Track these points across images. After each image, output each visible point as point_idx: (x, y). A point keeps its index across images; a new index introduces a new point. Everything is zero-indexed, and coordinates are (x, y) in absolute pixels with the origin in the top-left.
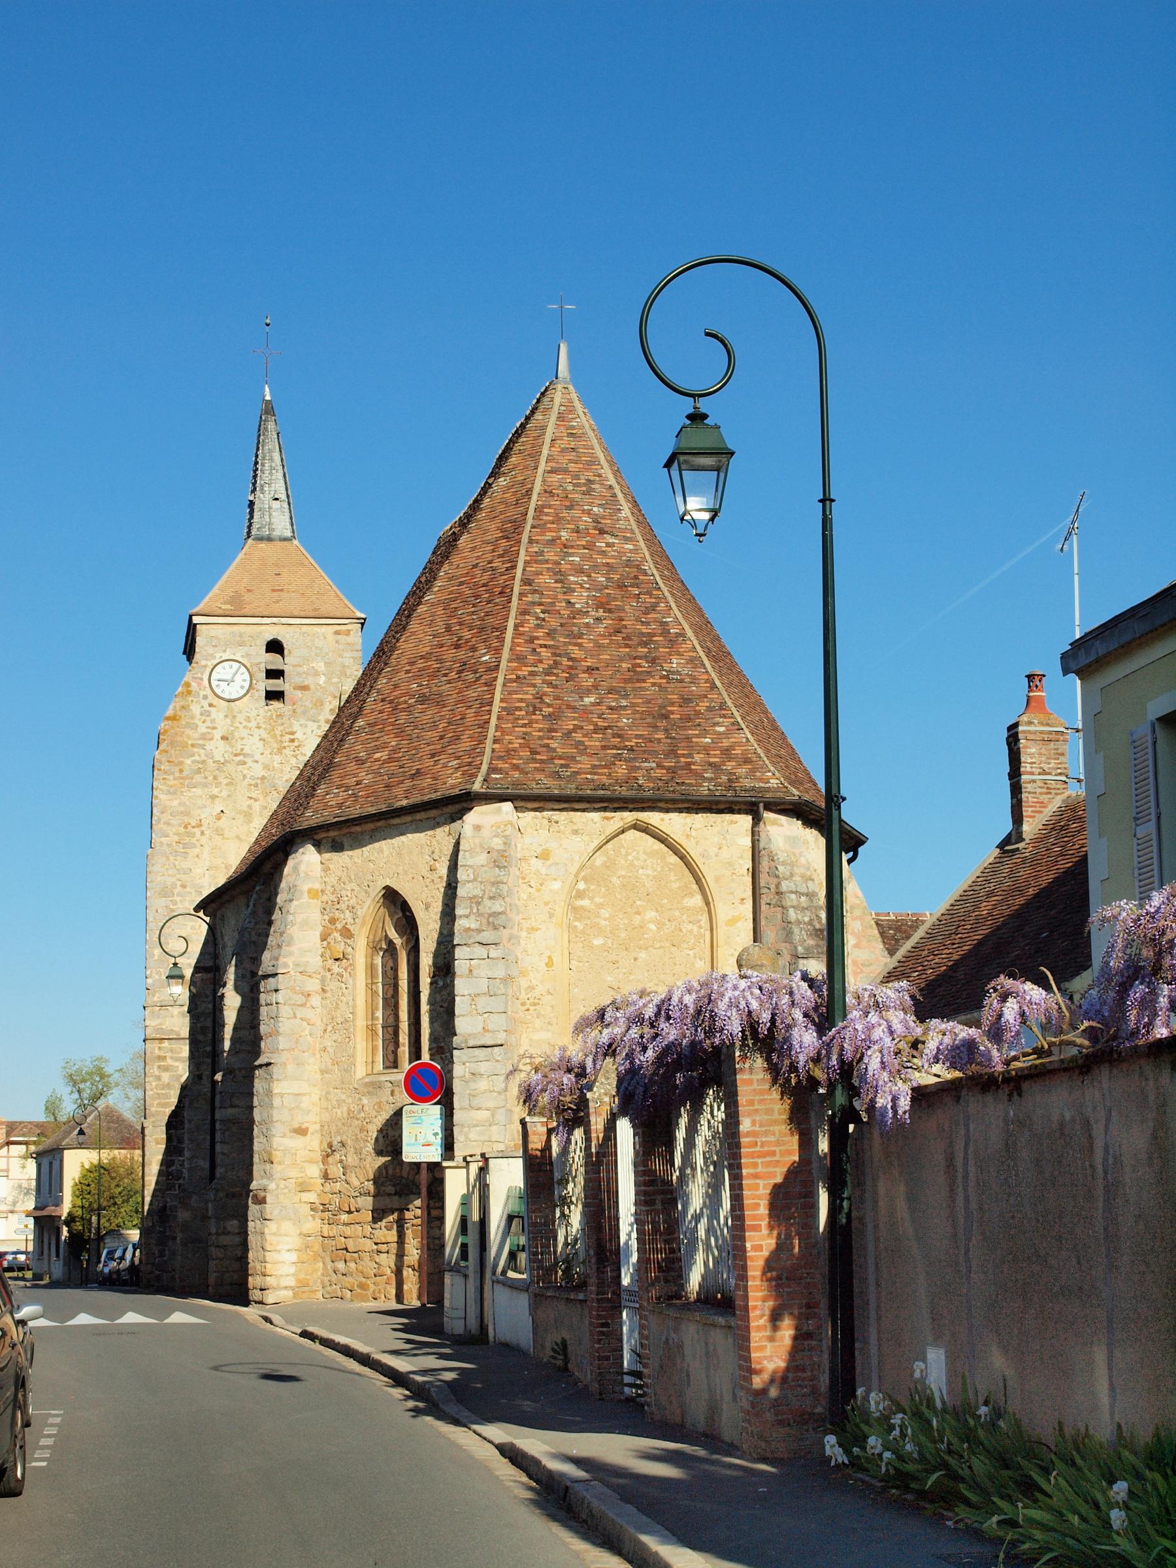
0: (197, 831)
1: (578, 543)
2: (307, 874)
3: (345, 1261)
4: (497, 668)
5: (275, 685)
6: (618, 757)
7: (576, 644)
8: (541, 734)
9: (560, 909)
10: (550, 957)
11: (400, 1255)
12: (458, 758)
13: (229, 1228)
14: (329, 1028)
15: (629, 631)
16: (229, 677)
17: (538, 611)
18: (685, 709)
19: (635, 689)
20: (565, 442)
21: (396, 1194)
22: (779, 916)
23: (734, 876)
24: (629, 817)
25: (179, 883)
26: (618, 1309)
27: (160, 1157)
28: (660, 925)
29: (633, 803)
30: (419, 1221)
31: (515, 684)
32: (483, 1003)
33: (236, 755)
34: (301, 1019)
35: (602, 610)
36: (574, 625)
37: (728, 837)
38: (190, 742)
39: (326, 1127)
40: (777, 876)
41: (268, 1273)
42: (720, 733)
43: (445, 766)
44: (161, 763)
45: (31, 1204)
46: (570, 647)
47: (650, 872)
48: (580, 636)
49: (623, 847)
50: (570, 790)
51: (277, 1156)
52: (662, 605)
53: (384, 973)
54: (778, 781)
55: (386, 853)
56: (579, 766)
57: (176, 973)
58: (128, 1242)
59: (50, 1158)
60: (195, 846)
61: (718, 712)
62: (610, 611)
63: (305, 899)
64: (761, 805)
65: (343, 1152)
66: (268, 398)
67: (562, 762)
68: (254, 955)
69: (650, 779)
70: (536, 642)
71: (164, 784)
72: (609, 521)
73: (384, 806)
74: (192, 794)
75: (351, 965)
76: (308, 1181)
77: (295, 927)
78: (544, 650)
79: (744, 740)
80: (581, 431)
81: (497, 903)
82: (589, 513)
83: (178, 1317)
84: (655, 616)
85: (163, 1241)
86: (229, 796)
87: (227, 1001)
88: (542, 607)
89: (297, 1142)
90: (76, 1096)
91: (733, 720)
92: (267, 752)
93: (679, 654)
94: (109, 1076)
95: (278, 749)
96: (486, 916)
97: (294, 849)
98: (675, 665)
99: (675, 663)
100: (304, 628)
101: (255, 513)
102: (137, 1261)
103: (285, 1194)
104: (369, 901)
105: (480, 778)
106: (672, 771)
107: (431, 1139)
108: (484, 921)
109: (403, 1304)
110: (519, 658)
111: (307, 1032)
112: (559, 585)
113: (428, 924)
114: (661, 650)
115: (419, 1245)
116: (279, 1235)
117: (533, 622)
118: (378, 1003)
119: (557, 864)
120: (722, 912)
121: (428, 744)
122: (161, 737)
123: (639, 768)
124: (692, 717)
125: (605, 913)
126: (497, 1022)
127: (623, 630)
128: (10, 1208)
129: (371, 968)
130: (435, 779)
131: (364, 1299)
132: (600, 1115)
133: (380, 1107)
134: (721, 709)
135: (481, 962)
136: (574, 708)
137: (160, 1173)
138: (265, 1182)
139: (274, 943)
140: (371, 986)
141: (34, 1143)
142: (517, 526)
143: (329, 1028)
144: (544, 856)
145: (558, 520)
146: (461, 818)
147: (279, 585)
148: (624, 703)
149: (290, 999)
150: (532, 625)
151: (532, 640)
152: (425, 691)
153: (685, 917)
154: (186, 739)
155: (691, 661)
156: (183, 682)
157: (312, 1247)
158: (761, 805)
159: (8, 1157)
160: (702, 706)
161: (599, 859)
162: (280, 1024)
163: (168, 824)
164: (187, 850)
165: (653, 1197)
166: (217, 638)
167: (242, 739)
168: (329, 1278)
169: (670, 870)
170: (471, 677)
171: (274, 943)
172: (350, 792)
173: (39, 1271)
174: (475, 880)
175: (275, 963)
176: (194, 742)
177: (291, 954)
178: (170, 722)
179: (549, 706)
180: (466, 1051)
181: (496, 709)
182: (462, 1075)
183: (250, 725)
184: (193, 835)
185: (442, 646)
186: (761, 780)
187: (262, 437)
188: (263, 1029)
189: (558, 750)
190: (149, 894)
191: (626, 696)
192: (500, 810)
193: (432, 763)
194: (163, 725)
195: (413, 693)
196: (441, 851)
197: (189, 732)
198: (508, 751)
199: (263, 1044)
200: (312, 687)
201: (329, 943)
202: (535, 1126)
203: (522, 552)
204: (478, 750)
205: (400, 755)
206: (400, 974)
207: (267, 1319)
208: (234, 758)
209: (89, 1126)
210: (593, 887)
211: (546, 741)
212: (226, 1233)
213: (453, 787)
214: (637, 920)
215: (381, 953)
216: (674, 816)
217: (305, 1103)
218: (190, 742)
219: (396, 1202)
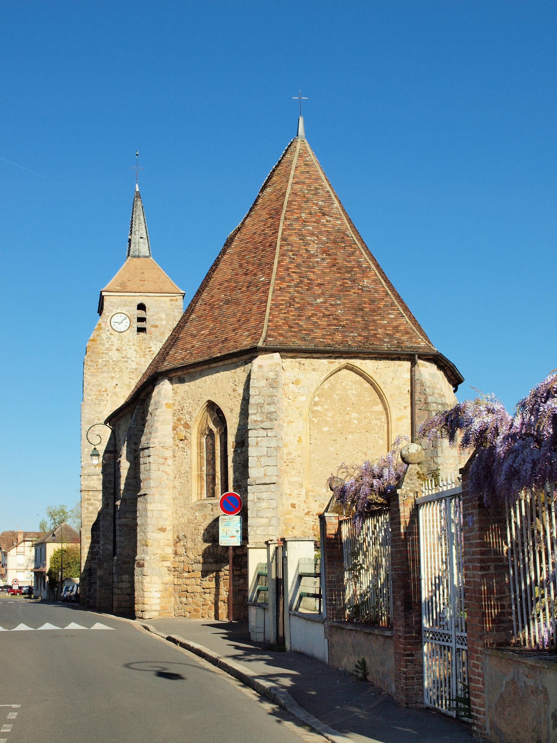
0: (105, 394)
1: (311, 220)
2: (165, 395)
3: (187, 597)
4: (269, 283)
5: (141, 325)
6: (337, 330)
7: (311, 272)
8: (294, 317)
9: (305, 411)
10: (299, 437)
11: (217, 594)
12: (248, 331)
13: (124, 579)
14: (177, 476)
15: (340, 265)
16: (120, 321)
17: (291, 254)
18: (372, 306)
19: (344, 295)
20: (303, 168)
21: (214, 563)
22: (426, 416)
23: (401, 395)
24: (343, 362)
25: (96, 418)
26: (420, 644)
27: (89, 545)
28: (360, 421)
29: (346, 354)
30: (228, 577)
31: (279, 292)
32: (264, 461)
33: (123, 358)
34: (162, 471)
35: (325, 255)
36: (310, 262)
37: (398, 373)
38: (101, 352)
39: (176, 528)
40: (425, 394)
41: (145, 603)
42: (392, 319)
43: (241, 335)
44: (87, 361)
45: (33, 567)
46: (308, 273)
47: (354, 392)
48: (314, 267)
49: (340, 378)
50: (311, 346)
51: (150, 542)
52: (357, 252)
53: (207, 447)
54: (425, 344)
55: (208, 383)
56: (316, 334)
57: (95, 453)
58: (75, 583)
59: (41, 547)
60: (103, 400)
61: (391, 308)
62: (329, 255)
63: (164, 408)
64: (417, 356)
65: (185, 541)
66: (137, 190)
67: (306, 332)
68: (136, 441)
69: (354, 342)
70: (290, 270)
71: (89, 371)
72: (327, 209)
73: (207, 357)
74: (102, 376)
75: (189, 443)
76: (166, 555)
77: (158, 423)
78: (295, 274)
79: (405, 322)
80: (311, 163)
81: (272, 407)
82: (317, 204)
83: (98, 626)
84: (354, 258)
85: (90, 584)
86: (120, 377)
87: (122, 464)
88: (293, 253)
89: (161, 535)
90: (53, 521)
91: (398, 312)
92: (138, 356)
93: (368, 277)
94: (67, 513)
95: (143, 355)
96: (266, 414)
97: (157, 383)
98: (365, 283)
99: (366, 282)
100: (156, 298)
101: (132, 245)
102: (78, 592)
103: (154, 562)
104: (199, 408)
105: (262, 340)
106: (367, 338)
107: (235, 534)
108: (265, 417)
109: (218, 620)
110: (281, 279)
111: (165, 478)
112: (302, 241)
113: (232, 420)
114: (358, 275)
115: (227, 590)
116: (152, 583)
117: (288, 260)
118: (203, 463)
119: (304, 387)
120: (394, 413)
121: (231, 325)
122: (87, 349)
123: (348, 336)
124: (376, 310)
125: (330, 414)
126: (271, 471)
127: (337, 265)
128: (26, 568)
129: (200, 444)
130: (236, 342)
131: (197, 617)
132: (407, 505)
133: (205, 517)
134: (392, 306)
135: (263, 438)
136: (312, 304)
137: (89, 553)
138: (143, 556)
139: (147, 432)
140: (200, 454)
141: (35, 541)
142: (278, 212)
143: (177, 476)
144: (297, 382)
145: (300, 208)
146: (251, 362)
147: (143, 278)
148: (339, 302)
149: (156, 460)
150: (288, 262)
151: (288, 269)
152: (229, 298)
153: (373, 416)
154: (99, 350)
155: (374, 281)
156: (98, 323)
157: (169, 590)
158: (417, 356)
159: (24, 547)
160: (381, 305)
161: (326, 385)
162: (151, 474)
163: (91, 390)
164: (100, 402)
165: (488, 564)
166: (114, 303)
167: (126, 350)
168: (178, 606)
169: (365, 391)
170: (254, 289)
171: (147, 432)
172: (188, 352)
173: (36, 595)
174: (259, 394)
175: (148, 442)
176: (103, 352)
177: (157, 437)
178: (92, 342)
179: (298, 303)
180: (255, 486)
181: (269, 304)
182: (252, 499)
183: (130, 344)
184: (103, 395)
185: (237, 275)
186: (416, 343)
187: (135, 209)
188: (142, 476)
189: (304, 326)
190: (82, 423)
191: (340, 299)
192: (272, 357)
193: (234, 334)
194: (88, 344)
195: (222, 300)
196: (239, 380)
197: (100, 347)
198: (276, 326)
199: (142, 484)
200: (159, 326)
201: (177, 432)
202: (331, 519)
203: (281, 224)
204: (260, 326)
205: (216, 331)
206: (216, 447)
207: (146, 628)
208: (123, 359)
209: (58, 533)
210: (323, 400)
211: (297, 321)
212: (122, 581)
213: (246, 345)
214: (347, 418)
215: (205, 437)
216: (368, 362)
217: (165, 515)
218: (101, 352)
219: (214, 567)
